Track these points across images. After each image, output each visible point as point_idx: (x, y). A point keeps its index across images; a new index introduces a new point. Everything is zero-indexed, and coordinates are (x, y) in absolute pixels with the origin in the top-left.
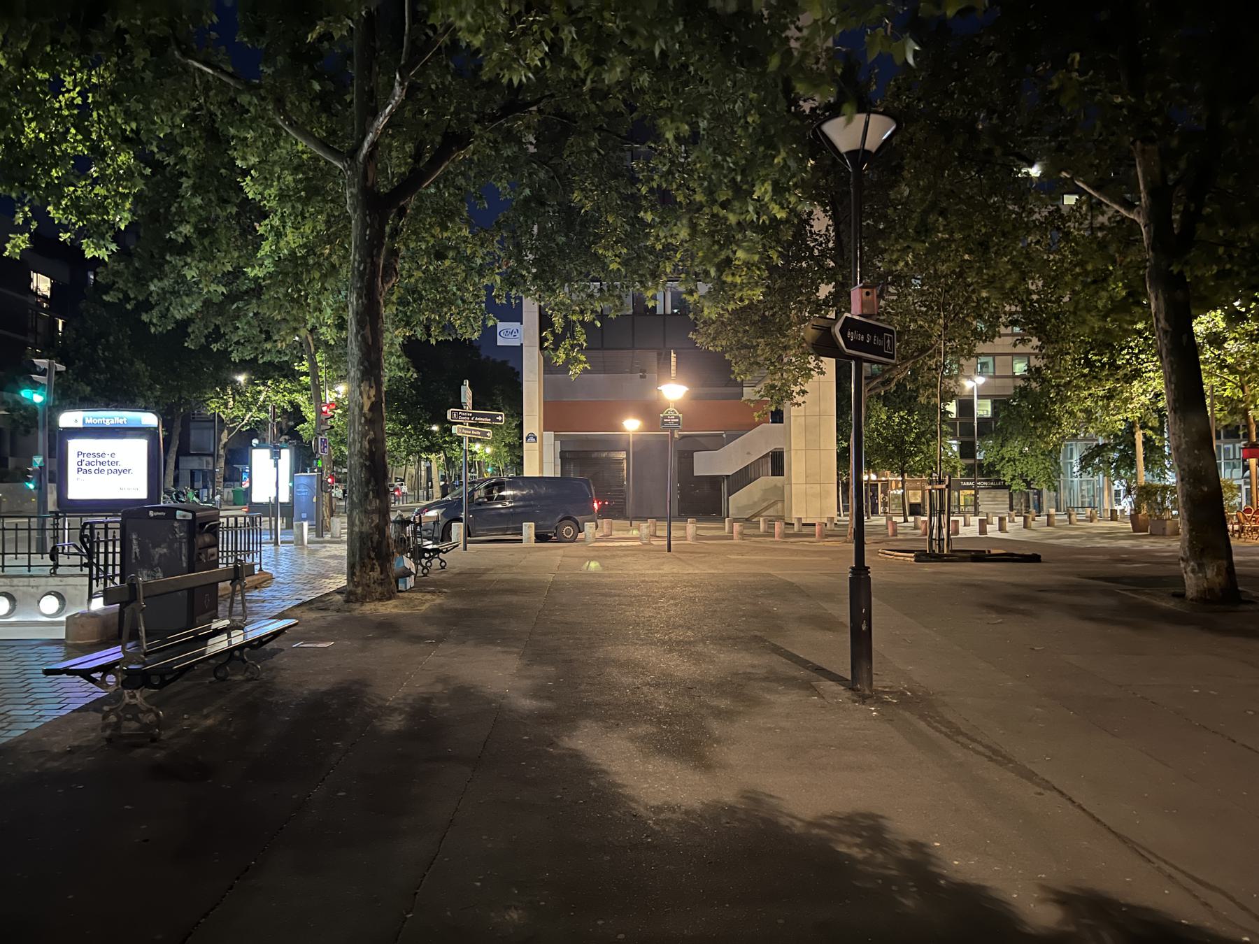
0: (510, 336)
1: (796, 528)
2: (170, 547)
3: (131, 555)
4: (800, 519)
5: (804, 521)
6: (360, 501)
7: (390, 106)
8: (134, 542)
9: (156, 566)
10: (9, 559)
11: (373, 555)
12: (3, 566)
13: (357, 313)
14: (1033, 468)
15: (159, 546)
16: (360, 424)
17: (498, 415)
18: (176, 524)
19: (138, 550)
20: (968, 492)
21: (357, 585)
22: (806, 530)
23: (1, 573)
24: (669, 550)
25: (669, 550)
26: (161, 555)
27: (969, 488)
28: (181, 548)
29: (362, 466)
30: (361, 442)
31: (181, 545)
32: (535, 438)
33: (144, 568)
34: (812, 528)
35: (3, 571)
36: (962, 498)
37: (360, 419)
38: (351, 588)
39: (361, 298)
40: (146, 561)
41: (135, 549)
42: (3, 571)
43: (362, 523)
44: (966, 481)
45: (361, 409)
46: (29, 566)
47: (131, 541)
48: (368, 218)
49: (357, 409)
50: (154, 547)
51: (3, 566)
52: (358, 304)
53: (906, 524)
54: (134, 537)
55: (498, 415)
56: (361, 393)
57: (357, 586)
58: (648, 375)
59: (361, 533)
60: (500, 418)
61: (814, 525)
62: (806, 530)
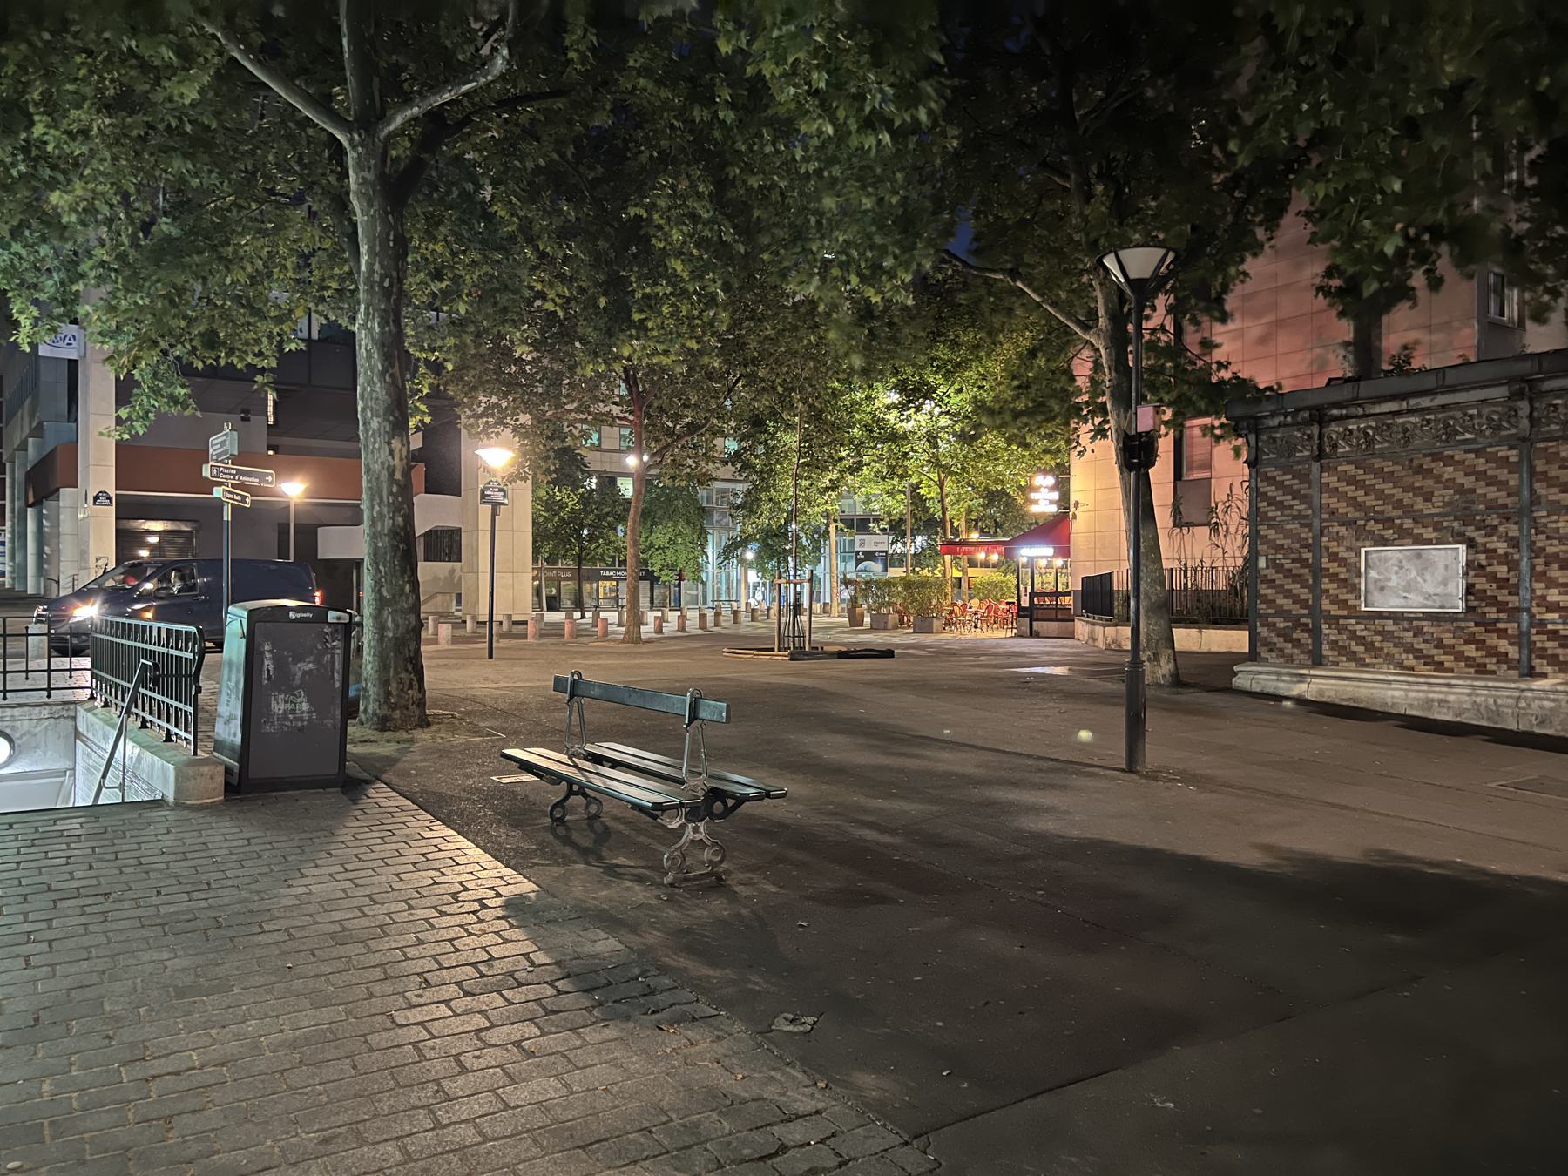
0: (61, 344)
1: (505, 627)
2: (318, 661)
3: (261, 671)
4: (509, 616)
5: (515, 618)
6: (394, 596)
7: (474, 84)
8: (267, 655)
9: (298, 687)
10: (15, 681)
11: (410, 668)
12: (5, 691)
13: (383, 345)
14: (682, 555)
15: (302, 660)
16: (391, 493)
17: (267, 475)
18: (327, 629)
19: (271, 667)
20: (608, 583)
21: (393, 708)
22: (517, 629)
23: (3, 702)
24: (491, 657)
25: (491, 657)
26: (305, 673)
27: (609, 578)
28: (333, 663)
29: (395, 549)
30: (393, 518)
31: (333, 657)
32: (109, 498)
33: (280, 691)
34: (524, 626)
35: (5, 698)
36: (601, 590)
37: (390, 486)
38: (385, 711)
39: (388, 324)
40: (283, 682)
41: (268, 664)
42: (5, 698)
43: (397, 625)
44: (605, 570)
45: (392, 473)
46: (49, 689)
47: (262, 653)
48: (390, 217)
49: (385, 473)
50: (296, 661)
51: (5, 691)
52: (382, 333)
53: (583, 621)
54: (267, 648)
55: (267, 475)
56: (391, 453)
57: (394, 710)
58: (252, 418)
59: (396, 638)
60: (270, 479)
61: (525, 623)
62: (517, 629)
